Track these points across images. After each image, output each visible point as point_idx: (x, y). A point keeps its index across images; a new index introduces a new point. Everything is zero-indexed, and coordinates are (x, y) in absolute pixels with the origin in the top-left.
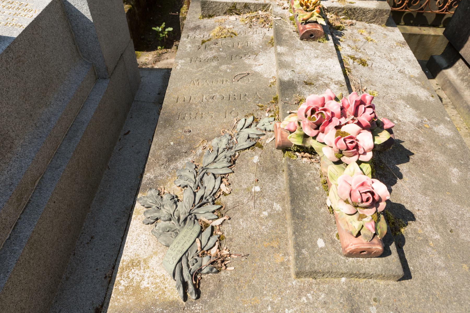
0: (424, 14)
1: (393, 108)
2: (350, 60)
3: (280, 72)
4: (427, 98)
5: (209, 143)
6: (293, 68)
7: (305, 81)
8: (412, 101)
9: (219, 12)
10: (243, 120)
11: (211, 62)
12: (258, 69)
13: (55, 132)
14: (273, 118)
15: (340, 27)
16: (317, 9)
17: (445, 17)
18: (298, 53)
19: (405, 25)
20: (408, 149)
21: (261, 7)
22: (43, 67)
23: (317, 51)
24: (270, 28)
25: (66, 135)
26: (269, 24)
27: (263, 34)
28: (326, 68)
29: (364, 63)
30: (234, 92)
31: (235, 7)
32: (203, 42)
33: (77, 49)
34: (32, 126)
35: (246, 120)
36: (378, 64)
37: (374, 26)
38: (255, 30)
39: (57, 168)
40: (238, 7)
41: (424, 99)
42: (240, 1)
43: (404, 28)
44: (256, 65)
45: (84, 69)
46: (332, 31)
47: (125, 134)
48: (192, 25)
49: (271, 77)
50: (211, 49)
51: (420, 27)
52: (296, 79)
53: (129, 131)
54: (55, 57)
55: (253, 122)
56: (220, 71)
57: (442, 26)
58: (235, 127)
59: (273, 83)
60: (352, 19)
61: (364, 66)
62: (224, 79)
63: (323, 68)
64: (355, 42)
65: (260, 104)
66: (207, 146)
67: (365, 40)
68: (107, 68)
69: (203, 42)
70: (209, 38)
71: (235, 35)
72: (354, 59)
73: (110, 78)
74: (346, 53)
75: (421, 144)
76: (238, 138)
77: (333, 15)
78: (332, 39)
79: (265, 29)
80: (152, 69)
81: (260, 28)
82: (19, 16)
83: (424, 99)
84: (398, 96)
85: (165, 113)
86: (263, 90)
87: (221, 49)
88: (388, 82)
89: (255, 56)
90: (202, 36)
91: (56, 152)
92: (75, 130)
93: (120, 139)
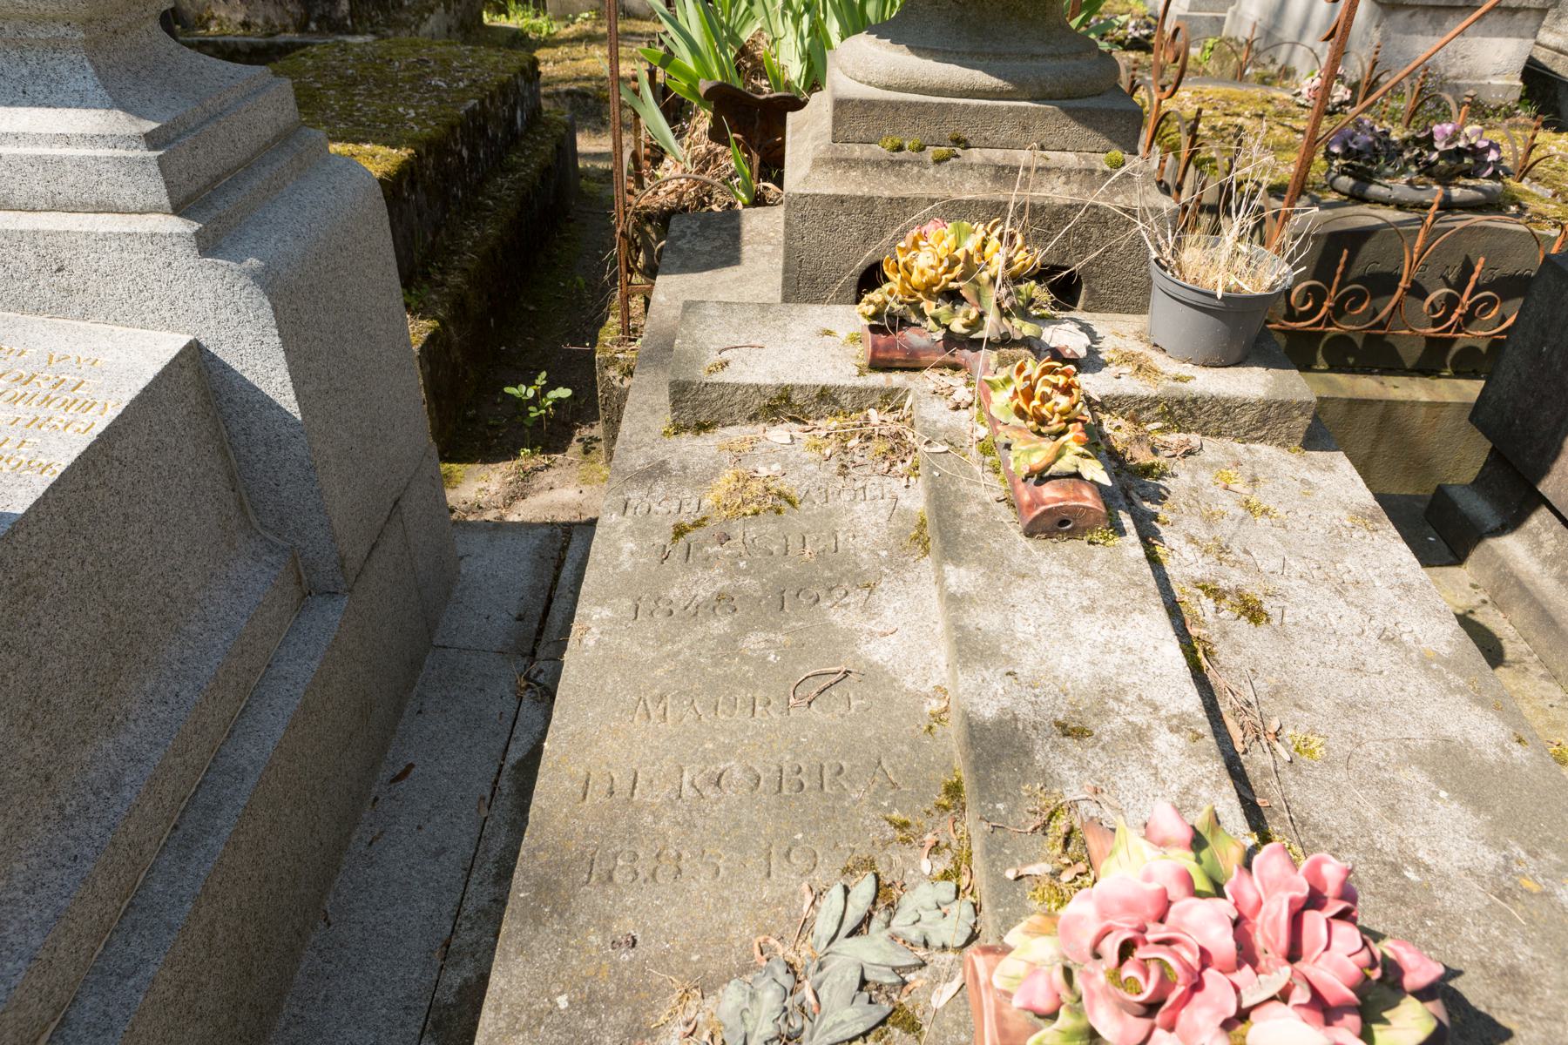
0: (1388, 339)
1: (1391, 808)
2: (1203, 599)
3: (966, 682)
4: (1504, 750)
5: (710, 1002)
6: (1009, 659)
7: (1060, 717)
8: (1452, 766)
9: (731, 415)
10: (837, 892)
11: (706, 616)
12: (879, 652)
13: (131, 828)
14: (952, 886)
15: (1153, 466)
16: (1075, 430)
17: (1456, 347)
18: (1022, 593)
19: (1331, 369)
20: (1483, 1009)
21: (877, 398)
22: (110, 593)
23: (1089, 582)
24: (912, 479)
25: (176, 827)
26: (909, 462)
27: (887, 500)
28: (1130, 658)
29: (1254, 613)
30: (796, 755)
31: (788, 399)
32: (680, 531)
33: (242, 504)
34: (47, 818)
35: (847, 890)
36: (1304, 611)
37: (1264, 450)
38: (859, 484)
39: (123, 977)
40: (797, 398)
41: (1491, 754)
42: (803, 382)
43: (1329, 383)
44: (871, 633)
45: (262, 571)
46: (1132, 492)
47: (397, 779)
48: (638, 461)
49: (928, 688)
50: (708, 562)
51: (1380, 378)
52: (1024, 711)
53: (411, 766)
54: (160, 548)
55: (874, 903)
56: (745, 659)
57: (1448, 371)
58: (806, 926)
59: (937, 717)
60: (1189, 431)
61: (1257, 623)
62: (760, 695)
63: (1115, 658)
64: (1210, 520)
65: (896, 814)
66: (700, 1017)
67: (1241, 512)
68: (343, 559)
69: (680, 531)
70: (699, 516)
71: (792, 503)
72: (1217, 594)
73: (350, 591)
74: (1187, 571)
75: (1526, 979)
76: (820, 984)
77: (1121, 422)
78: (1134, 531)
79: (895, 482)
80: (500, 526)
81: (876, 479)
82: (44, 429)
83: (1492, 758)
84: (1398, 750)
85: (540, 848)
86: (906, 748)
87: (742, 564)
88: (1352, 687)
89: (866, 593)
90: (674, 508)
91: (131, 905)
92: (208, 807)
93: (376, 799)
